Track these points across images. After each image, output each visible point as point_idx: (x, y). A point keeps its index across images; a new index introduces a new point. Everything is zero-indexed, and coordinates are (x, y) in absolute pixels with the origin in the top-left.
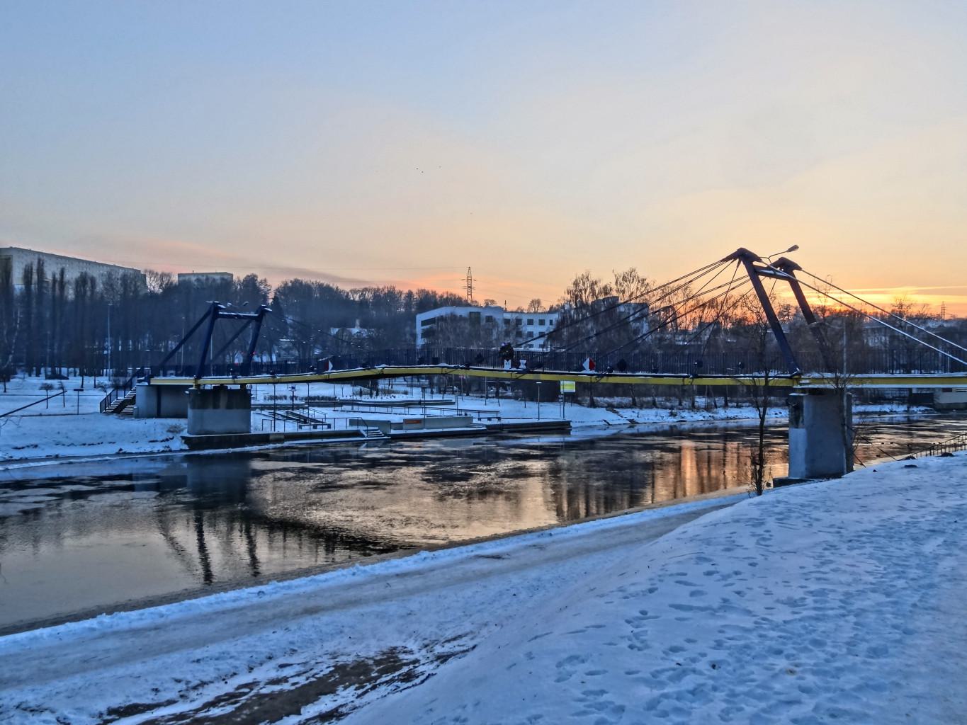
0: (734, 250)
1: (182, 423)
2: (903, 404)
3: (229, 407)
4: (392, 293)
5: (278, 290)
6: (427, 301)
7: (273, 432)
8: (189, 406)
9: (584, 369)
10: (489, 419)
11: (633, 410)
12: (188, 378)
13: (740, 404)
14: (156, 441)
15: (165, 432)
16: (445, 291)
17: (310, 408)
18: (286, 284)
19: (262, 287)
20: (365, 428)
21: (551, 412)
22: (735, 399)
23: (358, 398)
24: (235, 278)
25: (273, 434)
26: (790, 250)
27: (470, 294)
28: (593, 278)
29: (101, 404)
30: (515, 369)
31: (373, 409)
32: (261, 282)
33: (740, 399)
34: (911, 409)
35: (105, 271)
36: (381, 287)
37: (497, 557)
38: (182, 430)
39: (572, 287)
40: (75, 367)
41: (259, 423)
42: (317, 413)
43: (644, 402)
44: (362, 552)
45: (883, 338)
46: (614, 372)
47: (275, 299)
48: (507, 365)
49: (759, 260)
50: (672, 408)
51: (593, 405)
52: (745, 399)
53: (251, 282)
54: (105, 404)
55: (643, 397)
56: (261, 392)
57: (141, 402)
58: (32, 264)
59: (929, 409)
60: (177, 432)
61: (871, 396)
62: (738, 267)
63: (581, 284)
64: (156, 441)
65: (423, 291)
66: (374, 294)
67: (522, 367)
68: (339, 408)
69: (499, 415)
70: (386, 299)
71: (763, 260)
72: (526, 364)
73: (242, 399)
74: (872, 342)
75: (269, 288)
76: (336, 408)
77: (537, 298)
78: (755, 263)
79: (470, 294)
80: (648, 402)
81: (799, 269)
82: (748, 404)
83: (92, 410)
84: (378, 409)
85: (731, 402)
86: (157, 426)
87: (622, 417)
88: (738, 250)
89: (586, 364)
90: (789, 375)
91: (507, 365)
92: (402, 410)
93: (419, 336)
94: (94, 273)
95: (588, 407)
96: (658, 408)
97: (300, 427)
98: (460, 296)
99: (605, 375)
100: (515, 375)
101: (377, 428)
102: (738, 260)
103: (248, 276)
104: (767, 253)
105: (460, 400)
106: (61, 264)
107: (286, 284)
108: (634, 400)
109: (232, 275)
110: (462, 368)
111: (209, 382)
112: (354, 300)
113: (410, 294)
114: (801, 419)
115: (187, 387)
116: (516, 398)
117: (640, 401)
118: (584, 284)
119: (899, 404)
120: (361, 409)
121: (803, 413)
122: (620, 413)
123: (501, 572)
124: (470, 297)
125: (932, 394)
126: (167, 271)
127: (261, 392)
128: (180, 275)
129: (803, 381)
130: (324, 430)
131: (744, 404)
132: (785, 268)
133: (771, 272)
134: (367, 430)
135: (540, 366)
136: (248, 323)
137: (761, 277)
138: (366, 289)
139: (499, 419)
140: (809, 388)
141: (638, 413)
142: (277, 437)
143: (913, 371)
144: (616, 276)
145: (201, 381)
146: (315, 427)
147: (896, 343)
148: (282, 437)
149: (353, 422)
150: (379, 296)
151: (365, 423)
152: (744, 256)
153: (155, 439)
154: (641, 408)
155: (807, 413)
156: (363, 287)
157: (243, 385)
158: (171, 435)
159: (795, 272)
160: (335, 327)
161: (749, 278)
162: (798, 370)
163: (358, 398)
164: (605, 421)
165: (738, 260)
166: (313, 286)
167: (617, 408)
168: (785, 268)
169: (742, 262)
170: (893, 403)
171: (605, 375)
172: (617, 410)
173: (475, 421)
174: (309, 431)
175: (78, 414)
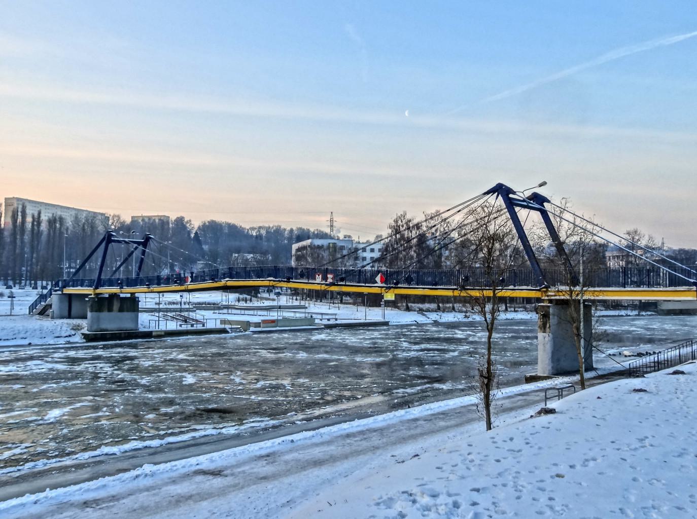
0: (492, 185)
1: (84, 323)
2: (635, 310)
3: (121, 310)
4: (279, 230)
5: (199, 228)
6: (302, 235)
7: (157, 329)
8: (88, 310)
9: (376, 283)
10: (329, 320)
11: (438, 313)
12: (89, 288)
13: (516, 309)
14: (61, 337)
15: (68, 329)
16: (316, 229)
17: (197, 311)
18: (205, 223)
19: (188, 225)
20: (230, 326)
21: (374, 314)
22: (513, 306)
23: (237, 303)
25: (157, 331)
26: (541, 185)
27: (332, 230)
28: (408, 217)
29: (29, 307)
30: (324, 282)
31: (243, 312)
32: (187, 222)
33: (517, 306)
34: (641, 313)
35: (73, 213)
36: (271, 226)
37: (216, 473)
38: (83, 328)
39: (393, 224)
40: (47, 281)
41: (145, 321)
42: (199, 315)
43: (446, 307)
45: (621, 262)
46: (399, 286)
47: (196, 233)
48: (319, 279)
49: (514, 193)
50: (466, 312)
51: (408, 309)
52: (520, 306)
53: (180, 222)
54: (32, 307)
55: (445, 303)
56: (147, 299)
57: (55, 307)
58: (18, 208)
59: (653, 313)
60: (79, 330)
61: (612, 304)
62: (496, 199)
63: (400, 222)
64: (61, 337)
65: (300, 229)
66: (266, 230)
67: (330, 280)
68: (217, 311)
69: (337, 317)
70: (276, 234)
71: (517, 193)
73: (132, 304)
74: (612, 264)
75: (192, 226)
76: (215, 311)
78: (511, 196)
79: (332, 230)
80: (449, 307)
81: (548, 201)
82: (522, 309)
83: (22, 312)
84: (247, 312)
85: (510, 307)
86: (64, 325)
87: (429, 318)
88: (497, 185)
89: (378, 279)
90: (538, 288)
91: (319, 279)
92: (265, 313)
95: (404, 311)
96: (456, 312)
97: (181, 325)
98: (327, 232)
99: (392, 287)
100: (323, 287)
101: (239, 327)
102: (497, 193)
103: (178, 218)
104: (522, 189)
105: (312, 305)
106: (38, 207)
107: (205, 223)
108: (439, 306)
109: (169, 217)
110: (284, 281)
111: (106, 291)
112: (252, 235)
113: (292, 230)
114: (548, 326)
115: (86, 295)
116: (354, 304)
117: (444, 307)
118: (402, 222)
119: (632, 310)
120: (234, 311)
121: (549, 320)
122: (428, 316)
123: (222, 492)
124: (332, 233)
125: (656, 302)
126: (117, 214)
127: (147, 299)
129: (550, 294)
130: (198, 328)
131: (519, 309)
132: (537, 201)
133: (525, 203)
134: (231, 328)
135: (342, 280)
137: (517, 209)
138: (260, 228)
139: (336, 319)
141: (441, 316)
142: (159, 333)
143: (642, 286)
144: (425, 216)
145: (98, 291)
146: (192, 325)
147: (630, 266)
148: (163, 333)
149: (223, 322)
150: (271, 232)
151: (230, 322)
152: (501, 190)
153: (60, 336)
154: (444, 311)
155: (553, 320)
156: (258, 225)
157: (133, 294)
158: (73, 332)
159: (545, 204)
160: (235, 253)
161: (506, 210)
162: (546, 283)
163: (237, 303)
164: (416, 321)
165: (497, 193)
166: (223, 225)
167: (426, 311)
168: (537, 201)
169: (500, 195)
170: (627, 309)
171: (392, 287)
172: (425, 313)
173: (317, 321)
174: (186, 329)
175: (11, 315)
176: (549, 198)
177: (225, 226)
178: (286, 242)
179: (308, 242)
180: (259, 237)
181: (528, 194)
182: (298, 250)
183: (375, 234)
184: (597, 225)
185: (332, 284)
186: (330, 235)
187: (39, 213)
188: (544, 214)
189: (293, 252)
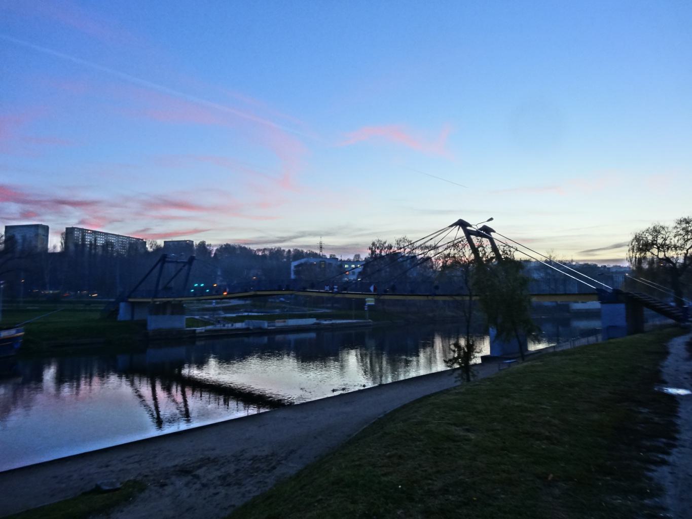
0: (456, 220)
3: (172, 313)
6: (298, 254)
24: (194, 244)
26: (489, 220)
32: (208, 245)
36: (273, 248)
44: (186, 419)
47: (215, 254)
49: (470, 226)
53: (202, 245)
71: (473, 226)
72: (337, 288)
77: (358, 254)
78: (468, 228)
81: (494, 231)
93: (292, 273)
94: (113, 240)
104: (476, 223)
109: (193, 242)
111: (158, 300)
113: (289, 251)
115: (149, 302)
128: (69, 233)
132: (486, 232)
135: (345, 289)
136: (184, 266)
137: (472, 237)
140: (351, 319)
152: (462, 224)
159: (492, 233)
165: (458, 226)
168: (486, 232)
176: (494, 229)
177: (238, 248)
178: (285, 260)
179: (303, 261)
180: (264, 256)
181: (480, 226)
182: (296, 267)
183: (353, 253)
184: (512, 247)
185: (337, 293)
186: (320, 255)
187: (95, 240)
188: (492, 241)
189: (292, 268)
